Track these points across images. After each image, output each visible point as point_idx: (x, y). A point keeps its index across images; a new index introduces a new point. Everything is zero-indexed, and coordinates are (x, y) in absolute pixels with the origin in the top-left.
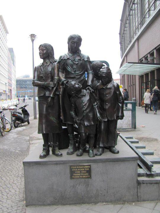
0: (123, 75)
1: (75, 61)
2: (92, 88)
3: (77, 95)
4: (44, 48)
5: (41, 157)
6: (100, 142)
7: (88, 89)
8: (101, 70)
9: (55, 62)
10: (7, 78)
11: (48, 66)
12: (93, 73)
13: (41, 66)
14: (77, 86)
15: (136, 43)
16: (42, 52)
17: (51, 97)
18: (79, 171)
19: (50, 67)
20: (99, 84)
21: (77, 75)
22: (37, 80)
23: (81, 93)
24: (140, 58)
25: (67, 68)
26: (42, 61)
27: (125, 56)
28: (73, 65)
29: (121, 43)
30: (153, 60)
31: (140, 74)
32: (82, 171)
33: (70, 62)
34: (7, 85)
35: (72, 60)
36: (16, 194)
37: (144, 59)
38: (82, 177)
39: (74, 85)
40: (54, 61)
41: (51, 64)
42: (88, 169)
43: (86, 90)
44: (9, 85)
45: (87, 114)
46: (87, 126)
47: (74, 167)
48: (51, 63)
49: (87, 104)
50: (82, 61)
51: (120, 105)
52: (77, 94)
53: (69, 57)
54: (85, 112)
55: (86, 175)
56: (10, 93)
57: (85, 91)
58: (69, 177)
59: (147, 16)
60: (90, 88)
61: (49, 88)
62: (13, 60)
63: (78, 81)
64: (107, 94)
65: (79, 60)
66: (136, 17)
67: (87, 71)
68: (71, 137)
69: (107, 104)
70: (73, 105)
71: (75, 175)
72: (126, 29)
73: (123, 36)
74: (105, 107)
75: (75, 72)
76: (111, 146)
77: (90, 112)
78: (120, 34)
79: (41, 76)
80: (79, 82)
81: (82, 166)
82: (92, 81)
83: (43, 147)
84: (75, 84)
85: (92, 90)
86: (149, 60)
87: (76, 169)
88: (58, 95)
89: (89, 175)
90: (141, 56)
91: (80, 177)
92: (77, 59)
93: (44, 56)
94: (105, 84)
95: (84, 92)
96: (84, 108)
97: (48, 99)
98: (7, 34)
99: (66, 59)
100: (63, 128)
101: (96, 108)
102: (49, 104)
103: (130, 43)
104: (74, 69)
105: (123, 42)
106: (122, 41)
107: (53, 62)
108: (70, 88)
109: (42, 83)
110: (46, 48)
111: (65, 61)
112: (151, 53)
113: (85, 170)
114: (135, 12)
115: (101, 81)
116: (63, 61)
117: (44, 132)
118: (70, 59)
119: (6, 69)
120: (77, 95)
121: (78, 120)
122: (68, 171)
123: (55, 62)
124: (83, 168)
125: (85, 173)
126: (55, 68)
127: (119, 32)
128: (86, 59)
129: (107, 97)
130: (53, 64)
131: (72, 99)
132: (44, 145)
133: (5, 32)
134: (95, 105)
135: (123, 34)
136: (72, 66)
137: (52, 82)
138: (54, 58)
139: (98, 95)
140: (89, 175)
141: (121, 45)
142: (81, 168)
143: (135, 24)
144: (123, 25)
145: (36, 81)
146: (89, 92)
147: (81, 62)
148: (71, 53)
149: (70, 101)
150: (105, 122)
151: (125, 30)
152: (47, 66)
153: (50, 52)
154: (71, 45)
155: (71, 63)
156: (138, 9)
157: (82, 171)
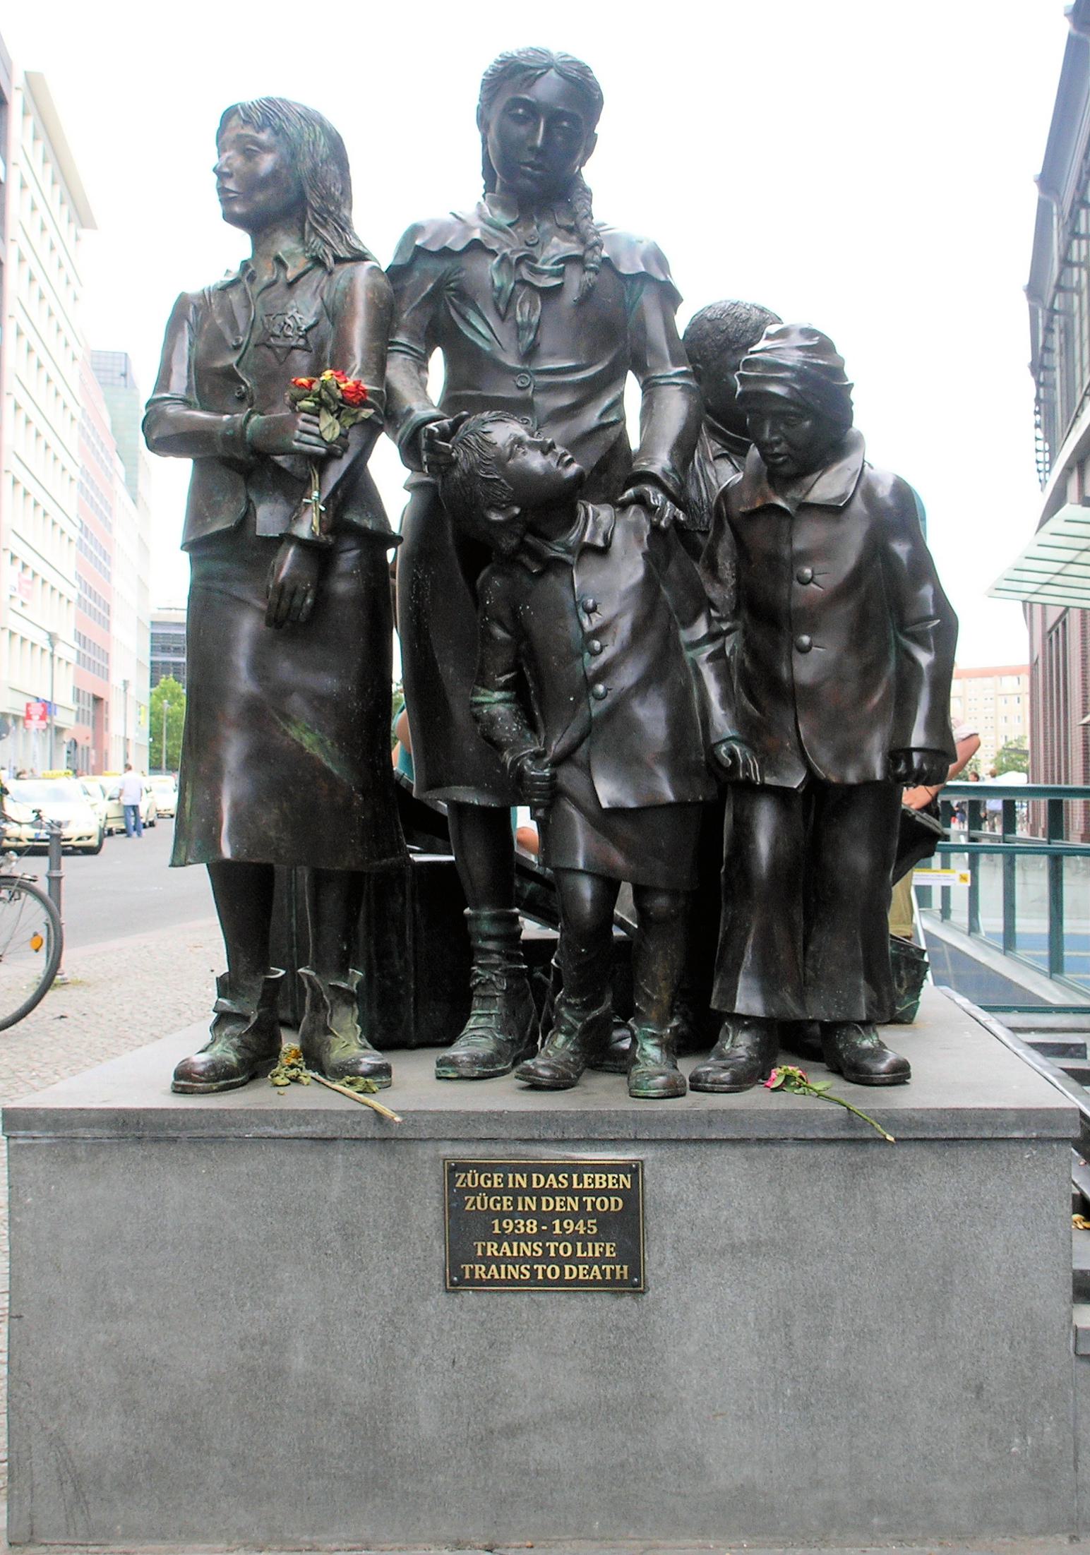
0: (1053, 615)
2: (669, 495)
3: (530, 539)
5: (185, 1080)
6: (742, 983)
10: (72, 594)
11: (291, 285)
12: (692, 383)
14: (536, 462)
16: (238, 162)
17: (302, 543)
18: (526, 1215)
22: (186, 403)
25: (462, 326)
26: (239, 245)
27: (1068, 469)
28: (510, 302)
29: (1038, 367)
32: (554, 1214)
33: (489, 272)
39: (512, 455)
40: (343, 252)
41: (319, 272)
42: (614, 1204)
44: (81, 658)
48: (318, 262)
50: (596, 272)
52: (532, 529)
53: (484, 232)
56: (88, 730)
58: (438, 1269)
65: (568, 260)
67: (640, 369)
68: (486, 927)
69: (806, 639)
70: (499, 633)
71: (492, 1249)
73: (1052, 311)
76: (837, 1015)
77: (642, 686)
78: (1033, 291)
79: (219, 364)
81: (557, 1169)
91: (534, 1273)
92: (551, 251)
93: (260, 197)
95: (597, 524)
96: (595, 654)
98: (84, 233)
99: (459, 247)
105: (1056, 360)
106: (1047, 349)
107: (338, 260)
108: (471, 474)
109: (226, 417)
111: (447, 265)
113: (582, 1205)
115: (754, 452)
116: (430, 265)
117: (227, 852)
119: (63, 522)
120: (530, 539)
121: (537, 756)
124: (569, 1192)
125: (585, 1239)
127: (1023, 276)
130: (336, 276)
132: (226, 986)
133: (61, 214)
135: (1059, 288)
138: (344, 226)
141: (1039, 384)
142: (553, 1193)
144: (1060, 216)
145: (172, 410)
148: (506, 207)
150: (782, 796)
151: (1075, 258)
152: (280, 289)
154: (503, 136)
155: (497, 283)
157: (562, 1216)
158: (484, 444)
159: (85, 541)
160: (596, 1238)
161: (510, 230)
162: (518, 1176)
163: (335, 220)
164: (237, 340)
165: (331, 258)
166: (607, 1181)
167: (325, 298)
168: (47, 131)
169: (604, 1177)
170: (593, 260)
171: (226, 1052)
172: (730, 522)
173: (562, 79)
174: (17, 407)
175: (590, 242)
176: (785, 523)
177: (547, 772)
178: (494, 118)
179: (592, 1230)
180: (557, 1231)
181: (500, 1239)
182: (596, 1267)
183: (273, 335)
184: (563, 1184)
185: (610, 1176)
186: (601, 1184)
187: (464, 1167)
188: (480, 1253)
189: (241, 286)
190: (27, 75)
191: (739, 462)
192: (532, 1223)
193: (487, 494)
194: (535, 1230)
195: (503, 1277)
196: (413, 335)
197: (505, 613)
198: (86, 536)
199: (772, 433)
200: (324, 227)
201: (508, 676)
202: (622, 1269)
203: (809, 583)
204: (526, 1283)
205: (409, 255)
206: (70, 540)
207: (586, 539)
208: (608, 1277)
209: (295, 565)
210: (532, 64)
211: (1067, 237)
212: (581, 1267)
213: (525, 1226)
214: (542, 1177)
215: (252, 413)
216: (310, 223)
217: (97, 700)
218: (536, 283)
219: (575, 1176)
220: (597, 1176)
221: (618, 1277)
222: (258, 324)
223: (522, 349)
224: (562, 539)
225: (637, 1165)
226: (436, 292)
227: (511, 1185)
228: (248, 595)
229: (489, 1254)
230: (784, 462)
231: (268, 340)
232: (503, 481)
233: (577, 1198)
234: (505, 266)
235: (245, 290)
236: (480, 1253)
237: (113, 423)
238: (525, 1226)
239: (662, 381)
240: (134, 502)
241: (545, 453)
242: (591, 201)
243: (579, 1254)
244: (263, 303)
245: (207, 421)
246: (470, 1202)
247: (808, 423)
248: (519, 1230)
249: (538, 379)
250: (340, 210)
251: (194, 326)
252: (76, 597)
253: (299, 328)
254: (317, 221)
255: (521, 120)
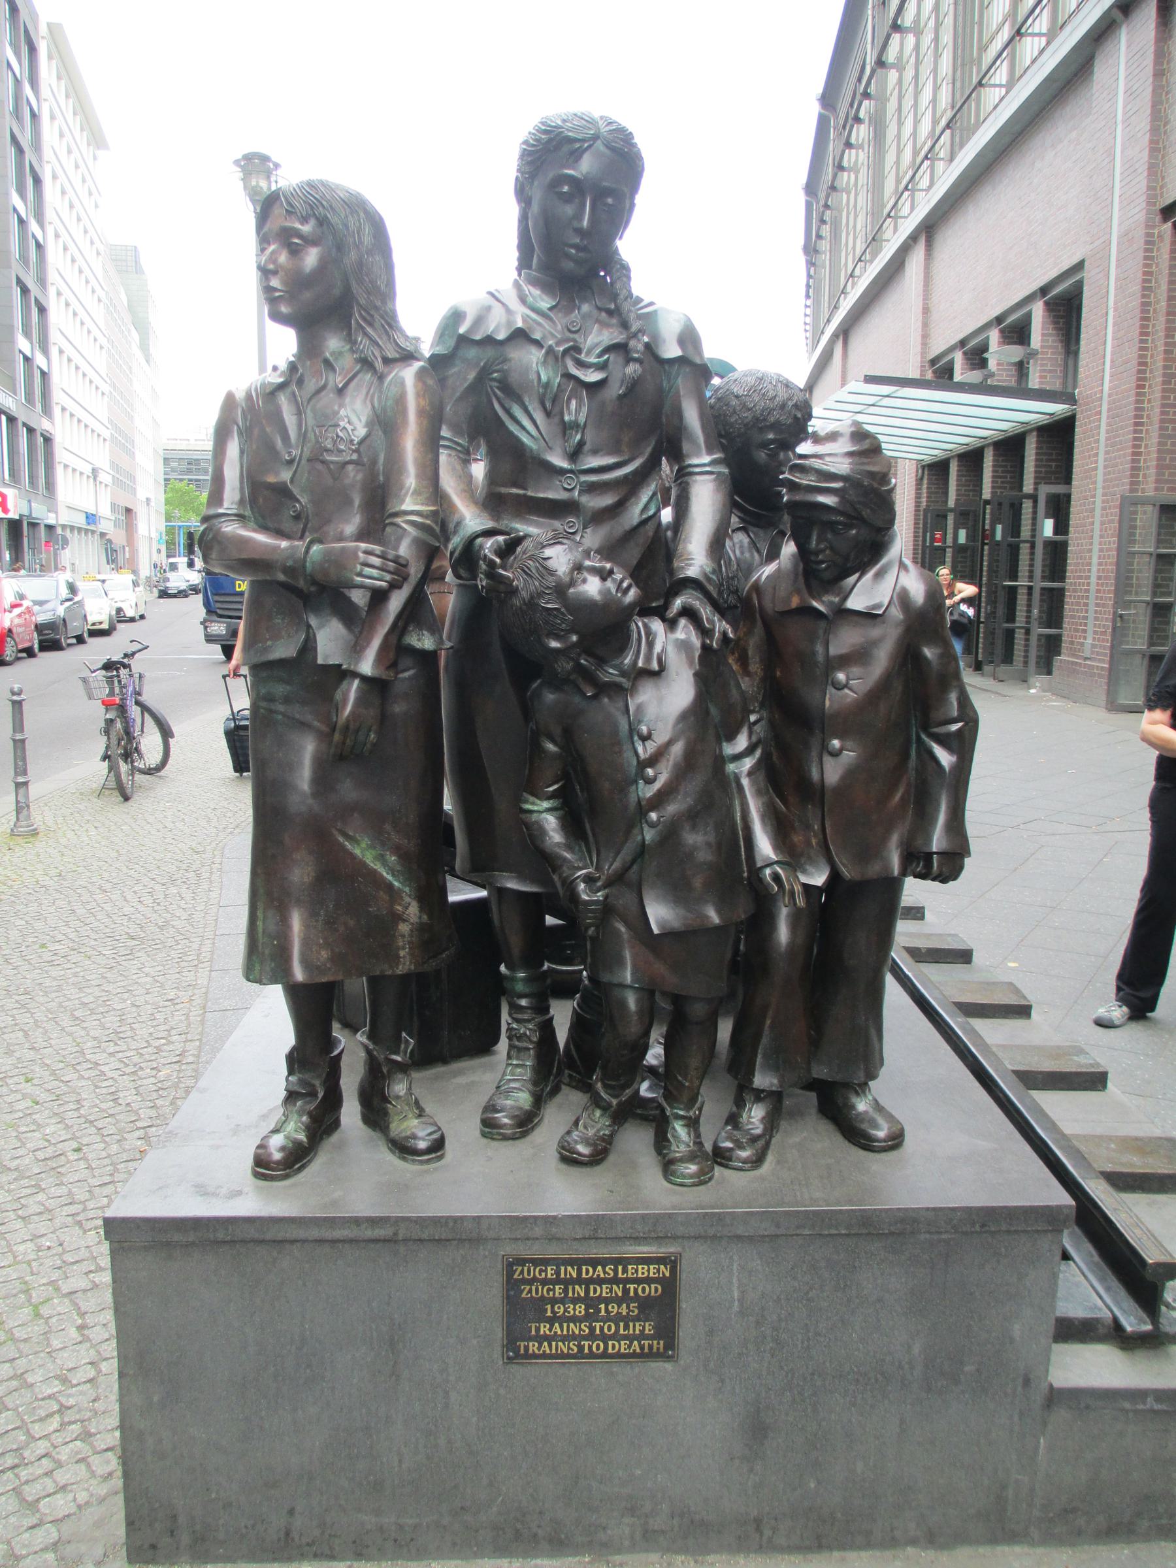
1: (581, 364)
4: (304, 220)
7: (688, 612)
8: (804, 448)
9: (408, 357)
13: (281, 387)
14: (592, 587)
15: (916, 259)
16: (283, 258)
17: (364, 679)
18: (575, 1301)
19: (358, 405)
20: (769, 570)
21: (591, 488)
22: (240, 517)
23: (622, 648)
24: (937, 348)
27: (835, 336)
30: (1021, 368)
31: (931, 453)
32: (600, 1299)
33: (530, 360)
34: (103, 477)
35: (550, 351)
36: (63, 1409)
37: (958, 358)
38: (598, 1346)
39: (572, 583)
40: (391, 354)
42: (654, 1290)
43: (671, 624)
45: (670, 834)
46: (670, 934)
47: (536, 1272)
49: (678, 749)
51: (945, 758)
54: (653, 816)
55: (630, 1338)
57: (657, 626)
59: (1001, 75)
60: (706, 612)
61: (346, 591)
62: (142, 328)
63: (592, 538)
64: (844, 661)
66: (922, 78)
69: (836, 743)
70: (551, 747)
71: (544, 1329)
72: (849, 157)
73: (826, 206)
74: (815, 774)
75: (574, 455)
79: (271, 479)
80: (609, 551)
82: (717, 546)
83: (291, 1072)
84: (578, 568)
85: (721, 626)
86: (992, 365)
87: (558, 1289)
88: (428, 659)
89: (657, 1336)
90: (944, 338)
91: (581, 1348)
92: (592, 339)
93: (307, 295)
94: (827, 575)
96: (650, 781)
97: (338, 695)
98: (99, 153)
99: (501, 336)
100: (453, 898)
101: (745, 782)
102: (337, 737)
103: (874, 255)
104: (566, 428)
106: (819, 237)
107: (387, 361)
108: (531, 604)
109: (284, 544)
110: (322, 222)
111: (490, 352)
112: (1074, 320)
113: (626, 1291)
114: (917, 47)
115: (789, 549)
116: (472, 353)
117: (299, 975)
118: (537, 336)
119: (97, 380)
122: (492, 1296)
123: (408, 357)
124: (615, 1280)
125: (626, 1320)
126: (404, 411)
128: (671, 351)
129: (839, 687)
131: (550, 697)
133: (82, 139)
134: (738, 757)
136: (552, 404)
137: (378, 549)
138: (390, 322)
139: (755, 666)
140: (657, 1336)
142: (600, 1282)
143: (917, 122)
145: (230, 528)
146: (696, 642)
147: (632, 369)
148: (546, 288)
149: (527, 711)
151: (845, 164)
152: (328, 397)
153: (360, 264)
155: (544, 378)
156: (938, 25)
158: (544, 571)
159: (114, 393)
160: (637, 1319)
161: (551, 315)
162: (569, 1268)
163: (382, 317)
164: (289, 453)
165: (380, 360)
166: (648, 1270)
167: (376, 405)
168: (68, 71)
169: (646, 1267)
170: (637, 346)
171: (296, 1130)
172: (762, 617)
173: (607, 152)
174: (61, 352)
175: (634, 329)
176: (823, 624)
177: (600, 896)
178: (537, 194)
179: (633, 1312)
180: (603, 1313)
181: (551, 1321)
182: (636, 1342)
183: (327, 450)
184: (609, 1274)
185: (651, 1267)
186: (643, 1273)
187: (522, 1262)
188: (533, 1332)
189: (289, 390)
190: (49, 25)
191: (754, 534)
192: (580, 1307)
193: (547, 623)
194: (583, 1312)
195: (554, 1351)
196: (456, 429)
197: (557, 731)
198: (114, 389)
199: (818, 543)
200: (371, 324)
201: (555, 787)
202: (658, 1344)
203: (843, 689)
204: (574, 1356)
205: (451, 343)
206: (103, 394)
207: (640, 664)
208: (646, 1350)
209: (360, 701)
210: (579, 136)
211: (841, 147)
212: (622, 1343)
213: (574, 1309)
214: (591, 1270)
215: (312, 542)
216: (357, 320)
217: (128, 511)
218: (583, 378)
219: (620, 1268)
220: (640, 1267)
221: (655, 1350)
222: (311, 436)
223: (570, 450)
224: (617, 662)
225: (676, 1257)
226: (478, 386)
227: (562, 1276)
228: (309, 718)
229: (542, 1332)
230: (826, 569)
231: (322, 455)
232: (563, 610)
233: (621, 1286)
234: (551, 360)
235: (294, 394)
236: (533, 1332)
237: (128, 301)
238: (574, 1309)
239: (697, 470)
240: (148, 361)
241: (604, 579)
242: (629, 278)
243: (622, 1332)
244: (314, 411)
245: (266, 545)
246: (517, 1273)
247: (854, 532)
248: (569, 1312)
249: (584, 478)
250: (386, 303)
251: (243, 431)
252: (109, 435)
253: (352, 441)
254: (365, 320)
255: (567, 199)
